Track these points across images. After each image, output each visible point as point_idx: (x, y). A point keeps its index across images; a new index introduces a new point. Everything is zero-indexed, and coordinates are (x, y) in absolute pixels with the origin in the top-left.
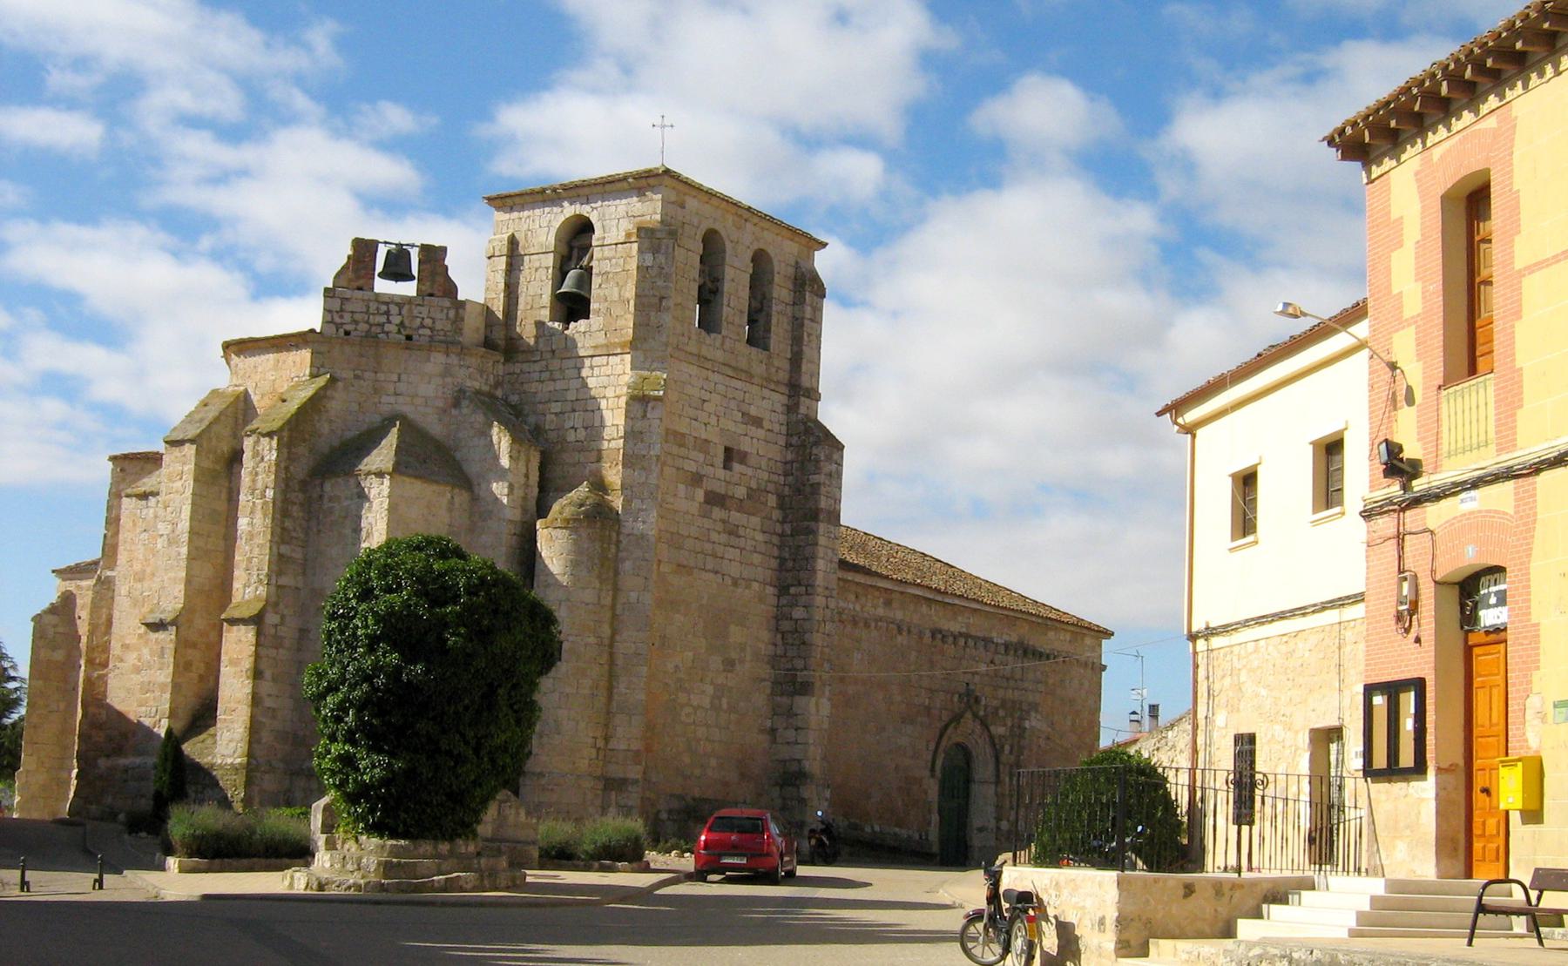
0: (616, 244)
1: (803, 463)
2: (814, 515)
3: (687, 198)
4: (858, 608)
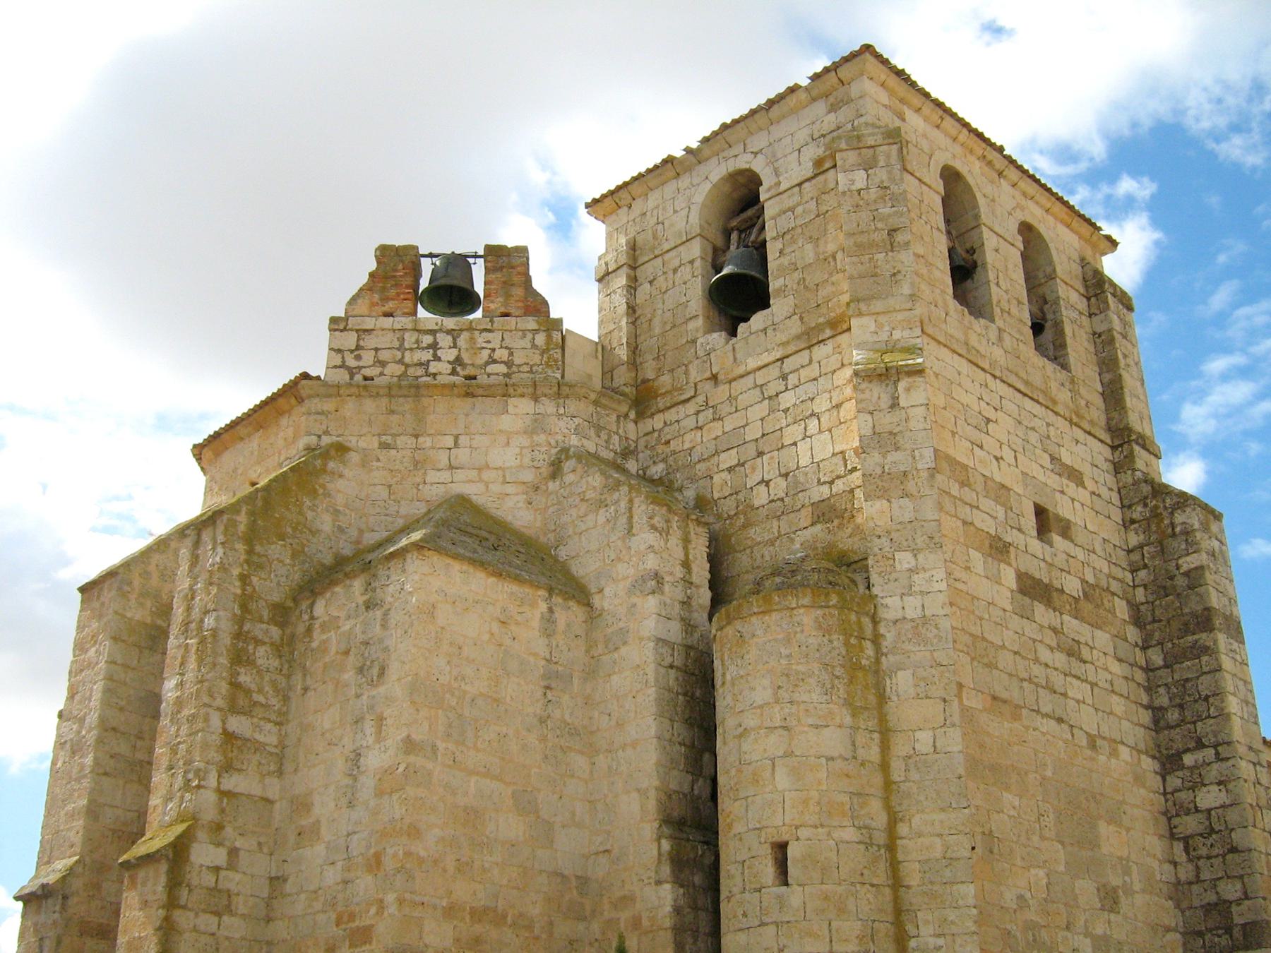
0: (800, 185)
1: (1161, 543)
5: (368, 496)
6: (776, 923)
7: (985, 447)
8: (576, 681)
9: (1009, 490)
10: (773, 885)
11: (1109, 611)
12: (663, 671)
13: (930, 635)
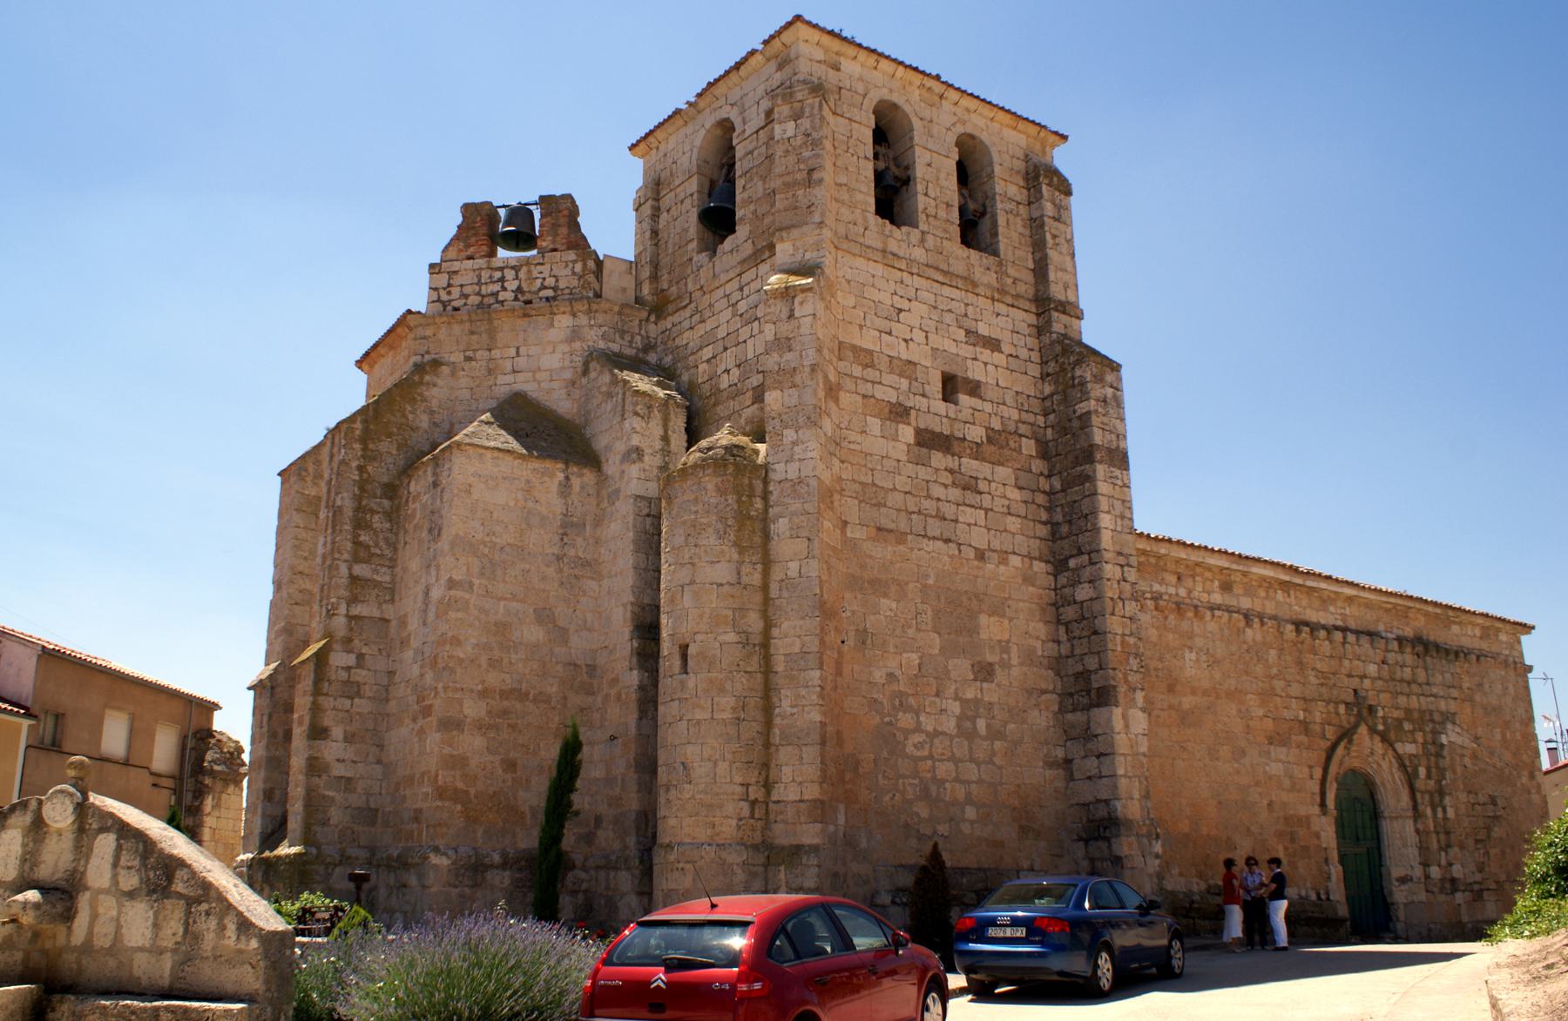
0: (757, 132)
1: (1064, 392)
2: (1088, 455)
3: (842, 60)
4: (1182, 592)
5: (456, 398)
6: (679, 699)
7: (893, 333)
8: (588, 527)
9: (915, 364)
10: (680, 674)
11: (1015, 450)
12: (640, 519)
13: (803, 491)
